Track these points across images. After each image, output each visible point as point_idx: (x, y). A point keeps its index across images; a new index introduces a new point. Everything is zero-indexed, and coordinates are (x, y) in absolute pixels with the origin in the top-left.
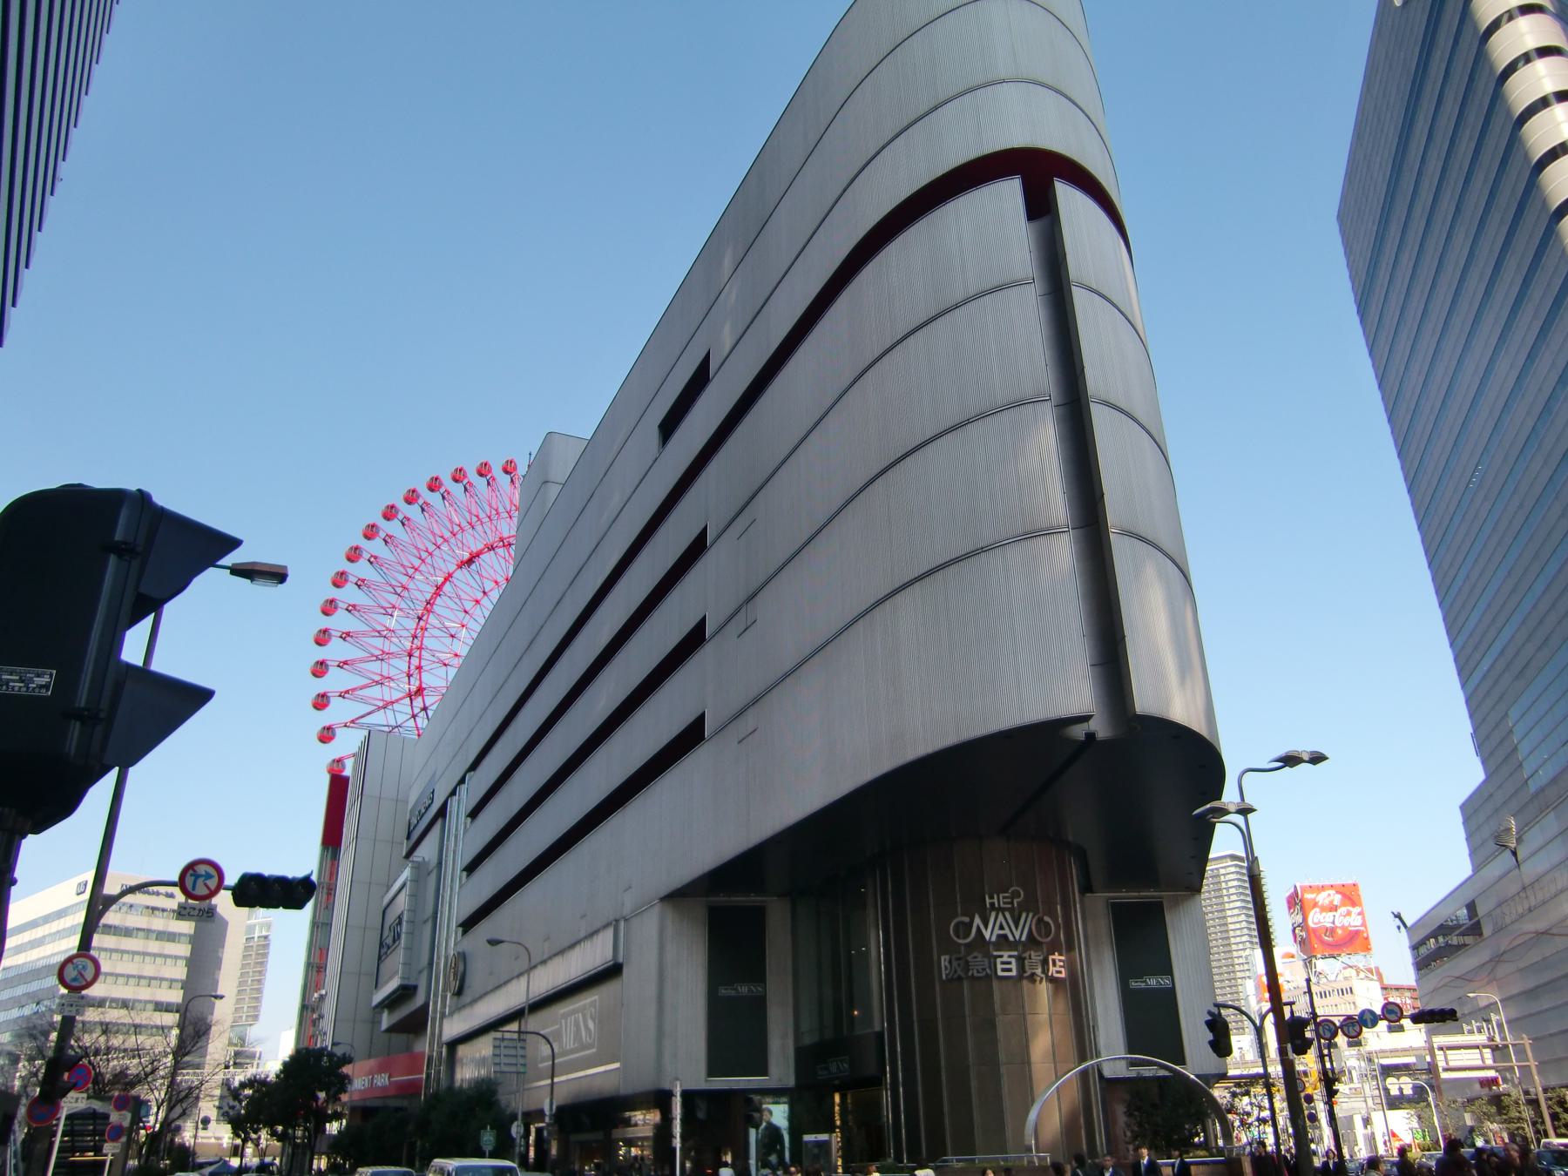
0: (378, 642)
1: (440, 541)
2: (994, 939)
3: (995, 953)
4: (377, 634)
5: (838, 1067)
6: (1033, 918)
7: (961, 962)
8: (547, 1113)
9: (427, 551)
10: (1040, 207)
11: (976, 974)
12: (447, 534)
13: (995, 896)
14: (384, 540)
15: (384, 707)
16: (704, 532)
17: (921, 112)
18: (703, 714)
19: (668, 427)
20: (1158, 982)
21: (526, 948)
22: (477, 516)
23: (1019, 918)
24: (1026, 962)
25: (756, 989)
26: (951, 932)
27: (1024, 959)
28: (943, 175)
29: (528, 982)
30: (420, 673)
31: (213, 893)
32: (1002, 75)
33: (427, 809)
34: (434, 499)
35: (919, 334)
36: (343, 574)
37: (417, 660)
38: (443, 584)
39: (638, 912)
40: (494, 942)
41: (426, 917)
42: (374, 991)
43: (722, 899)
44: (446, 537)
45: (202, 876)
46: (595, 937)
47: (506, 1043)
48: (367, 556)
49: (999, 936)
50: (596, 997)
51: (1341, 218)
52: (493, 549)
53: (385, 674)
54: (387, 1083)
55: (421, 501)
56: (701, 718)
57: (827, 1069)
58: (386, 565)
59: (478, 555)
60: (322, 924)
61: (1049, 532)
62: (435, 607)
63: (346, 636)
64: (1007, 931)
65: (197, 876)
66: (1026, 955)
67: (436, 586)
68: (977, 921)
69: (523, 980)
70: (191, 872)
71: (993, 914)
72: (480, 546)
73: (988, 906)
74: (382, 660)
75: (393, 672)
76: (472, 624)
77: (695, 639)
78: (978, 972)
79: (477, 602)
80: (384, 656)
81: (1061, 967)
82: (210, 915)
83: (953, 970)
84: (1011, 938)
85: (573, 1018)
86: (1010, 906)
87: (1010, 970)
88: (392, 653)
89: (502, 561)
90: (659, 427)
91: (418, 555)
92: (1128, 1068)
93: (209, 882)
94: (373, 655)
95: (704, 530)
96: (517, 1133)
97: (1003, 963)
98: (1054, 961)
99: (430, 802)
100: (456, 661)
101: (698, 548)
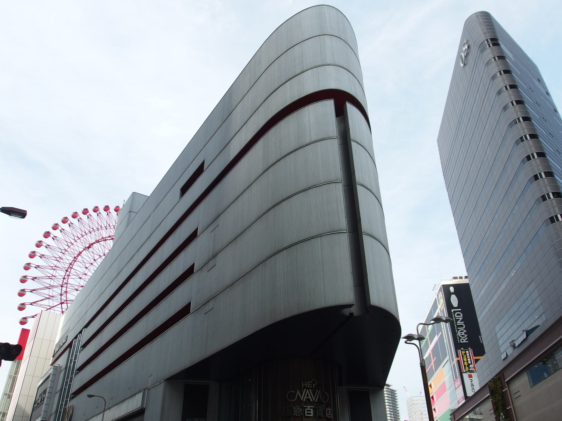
0: (51, 272)
1: (76, 239)
2: (304, 400)
3: (305, 406)
4: (48, 278)
6: (320, 392)
10: (341, 113)
11: (296, 415)
12: (80, 236)
13: (306, 382)
14: (53, 238)
16: (197, 230)
18: (190, 303)
19: (184, 190)
21: (104, 399)
23: (315, 392)
26: (287, 396)
27: (316, 409)
28: (304, 97)
30: (66, 294)
32: (328, 63)
35: (291, 155)
36: (34, 252)
37: (65, 288)
38: (82, 251)
40: (90, 396)
41: (57, 391)
46: (134, 397)
49: (306, 399)
51: (438, 141)
52: (99, 242)
55: (69, 222)
56: (189, 304)
58: (53, 249)
59: (92, 244)
61: (338, 232)
63: (37, 267)
64: (310, 397)
67: (74, 257)
68: (298, 393)
69: (101, 415)
71: (305, 390)
72: (94, 241)
73: (303, 386)
74: (50, 288)
77: (189, 272)
78: (297, 414)
79: (92, 264)
80: (50, 287)
81: (330, 413)
84: (311, 400)
86: (311, 387)
87: (310, 414)
88: (58, 267)
89: (102, 247)
90: (181, 189)
91: (67, 245)
95: (197, 229)
97: (307, 411)
99: (65, 341)
100: (104, 257)
101: (194, 236)
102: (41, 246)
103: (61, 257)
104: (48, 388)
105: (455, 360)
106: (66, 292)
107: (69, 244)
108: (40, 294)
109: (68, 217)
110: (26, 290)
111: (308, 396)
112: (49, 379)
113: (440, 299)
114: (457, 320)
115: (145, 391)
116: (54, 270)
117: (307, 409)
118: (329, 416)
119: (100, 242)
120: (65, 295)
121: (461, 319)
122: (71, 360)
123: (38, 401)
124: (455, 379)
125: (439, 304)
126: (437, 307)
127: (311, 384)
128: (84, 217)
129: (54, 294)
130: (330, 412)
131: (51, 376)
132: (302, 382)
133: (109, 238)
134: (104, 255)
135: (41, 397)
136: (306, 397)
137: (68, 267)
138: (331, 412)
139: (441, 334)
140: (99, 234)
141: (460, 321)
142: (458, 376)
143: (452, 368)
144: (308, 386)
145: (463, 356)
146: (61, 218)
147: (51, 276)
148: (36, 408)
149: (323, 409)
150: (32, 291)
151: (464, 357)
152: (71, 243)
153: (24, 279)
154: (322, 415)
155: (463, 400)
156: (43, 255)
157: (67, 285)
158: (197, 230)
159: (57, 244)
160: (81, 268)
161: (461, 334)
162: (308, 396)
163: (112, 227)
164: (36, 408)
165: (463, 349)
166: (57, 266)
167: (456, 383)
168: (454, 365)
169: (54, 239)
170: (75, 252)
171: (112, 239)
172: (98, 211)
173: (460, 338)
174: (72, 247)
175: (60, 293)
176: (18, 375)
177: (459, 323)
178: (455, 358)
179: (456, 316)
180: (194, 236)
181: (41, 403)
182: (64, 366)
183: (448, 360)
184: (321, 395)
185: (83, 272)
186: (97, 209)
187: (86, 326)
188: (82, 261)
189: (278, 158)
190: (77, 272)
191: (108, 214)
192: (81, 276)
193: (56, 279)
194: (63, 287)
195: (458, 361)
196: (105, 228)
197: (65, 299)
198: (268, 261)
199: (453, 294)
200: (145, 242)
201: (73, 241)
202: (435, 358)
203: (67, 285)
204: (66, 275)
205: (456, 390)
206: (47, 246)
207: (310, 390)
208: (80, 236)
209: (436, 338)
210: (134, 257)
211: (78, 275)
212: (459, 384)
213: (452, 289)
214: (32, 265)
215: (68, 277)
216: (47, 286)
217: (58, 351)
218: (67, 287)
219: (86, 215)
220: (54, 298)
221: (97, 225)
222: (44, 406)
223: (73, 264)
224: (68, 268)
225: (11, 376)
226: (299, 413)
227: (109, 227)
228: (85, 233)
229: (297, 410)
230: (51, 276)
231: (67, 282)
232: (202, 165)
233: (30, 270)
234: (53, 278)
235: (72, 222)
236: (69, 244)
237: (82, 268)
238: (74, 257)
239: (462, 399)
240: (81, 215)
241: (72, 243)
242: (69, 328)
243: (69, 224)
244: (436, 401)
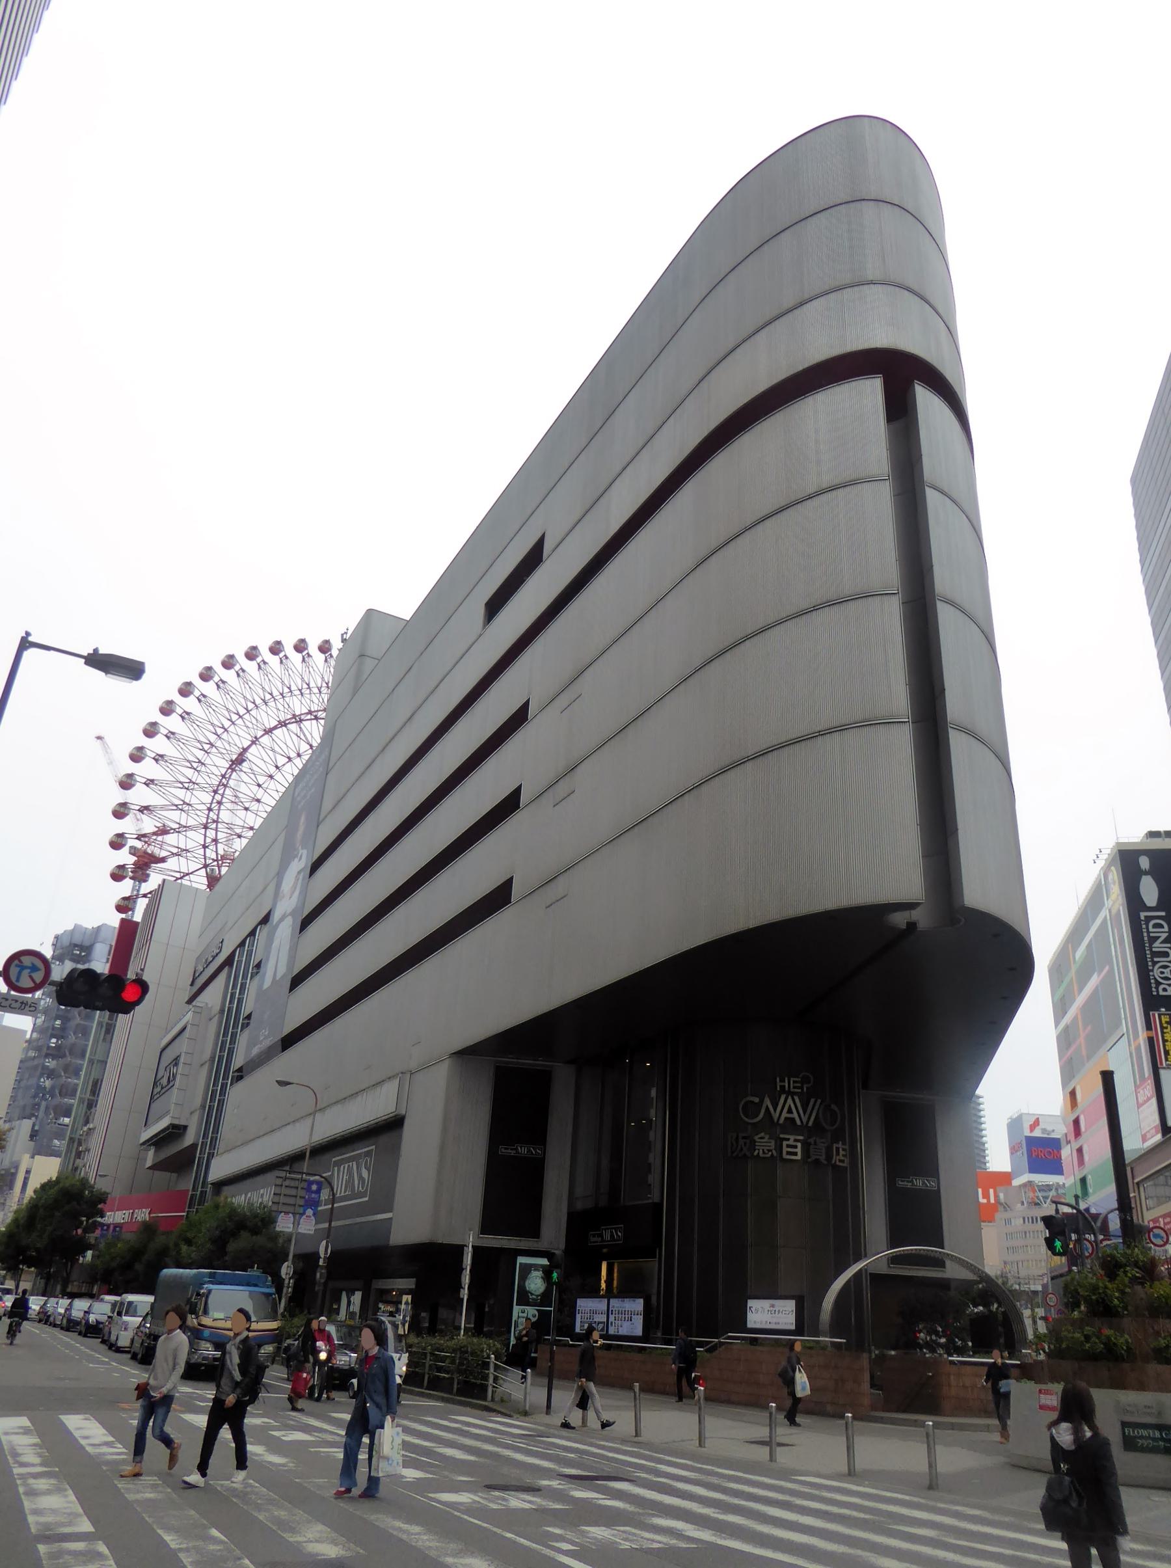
0: (181, 793)
2: (781, 1121)
3: (782, 1136)
4: (175, 808)
5: (612, 1236)
6: (821, 1104)
7: (748, 1141)
8: (322, 1255)
12: (242, 711)
13: (786, 1079)
16: (526, 705)
18: (512, 878)
19: (495, 606)
20: (924, 1183)
23: (807, 1105)
24: (812, 1147)
25: (536, 1151)
29: (313, 1122)
30: (216, 844)
33: (214, 958)
35: (768, 523)
36: (141, 749)
37: (220, 797)
38: (249, 747)
39: (424, 1067)
42: (144, 1129)
43: (510, 1060)
44: (257, 703)
45: (26, 967)
47: (287, 1183)
48: (180, 711)
49: (786, 1119)
51: (1135, 480)
52: (285, 725)
57: (601, 1235)
60: (98, 1061)
61: (889, 722)
63: (149, 783)
64: (795, 1115)
65: (22, 968)
66: (811, 1140)
67: (231, 761)
68: (767, 1102)
70: (16, 962)
71: (783, 1097)
72: (274, 723)
74: (179, 832)
76: (266, 799)
77: (510, 805)
78: (764, 1153)
79: (271, 777)
81: (843, 1155)
82: (33, 1009)
83: (739, 1147)
84: (798, 1122)
85: (347, 1165)
86: (800, 1091)
87: (796, 1154)
88: (197, 784)
89: (295, 737)
92: (889, 1267)
93: (35, 975)
97: (788, 1146)
98: (838, 1149)
99: (218, 951)
101: (519, 718)
103: (202, 761)
104: (183, 1054)
105: (1143, 1035)
106: (215, 841)
107: (220, 731)
109: (213, 667)
111: (790, 1111)
112: (184, 1033)
113: (1112, 886)
114: (1153, 940)
115: (407, 1075)
116: (187, 789)
117: (788, 1142)
118: (840, 1161)
119: (289, 726)
120: (212, 847)
121: (1164, 936)
122: (233, 995)
123: (161, 1081)
124: (1138, 1083)
125: (1107, 899)
126: (1104, 905)
127: (799, 1085)
128: (251, 667)
129: (190, 845)
130: (842, 1152)
131: (189, 1027)
132: (778, 1079)
133: (309, 717)
134: (299, 755)
135: (168, 1071)
136: (785, 1114)
137: (218, 783)
138: (844, 1153)
139: (1108, 972)
140: (286, 706)
141: (1159, 937)
142: (1147, 1075)
143: (1131, 1054)
144: (792, 1090)
145: (1162, 1028)
147: (182, 803)
148: (158, 1095)
149: (826, 1145)
151: (1165, 1031)
152: (223, 728)
153: (122, 810)
154: (823, 1158)
155: (1157, 1133)
156: (162, 756)
157: (217, 825)
158: (526, 705)
159: (192, 729)
160: (323, 820)
161: (1162, 973)
162: (790, 1111)
163: (316, 690)
164: (158, 1095)
165: (1163, 1010)
166: (194, 780)
167: (1141, 1091)
168: (1138, 1048)
169: (183, 718)
170: (233, 750)
171: (316, 718)
172: (281, 651)
173: (1158, 984)
174: (225, 736)
175: (203, 843)
176: (116, 1021)
177: (1158, 946)
178: (1143, 1032)
179: (1151, 929)
180: (519, 718)
181: (168, 1085)
182: (218, 1008)
183: (1123, 1035)
184: (820, 1112)
185: (253, 796)
188: (250, 771)
189: (735, 530)
191: (304, 660)
192: (247, 805)
193: (192, 812)
194: (208, 830)
195: (1151, 1041)
196: (298, 692)
197: (214, 856)
198: (704, 788)
199: (1146, 873)
200: (398, 732)
201: (227, 724)
202: (1089, 1028)
203: (217, 825)
204: (215, 801)
205: (1138, 1108)
206: (170, 735)
207: (796, 1098)
208: (242, 711)
209: (1094, 981)
211: (242, 802)
212: (1149, 1095)
213: (1144, 863)
214: (138, 778)
215: (219, 807)
216: (174, 827)
217: (201, 973)
219: (255, 662)
220: (188, 854)
221: (279, 685)
222: (175, 1091)
223: (230, 776)
224: (219, 785)
225: (102, 1022)
226: (769, 1151)
227: (308, 691)
228: (254, 705)
229: (764, 1144)
230: (182, 803)
231: (218, 818)
232: (540, 545)
233: (134, 789)
234: (186, 808)
235: (224, 680)
236: (220, 731)
239: (1154, 1130)
240: (265, 654)
241: (226, 727)
242: (226, 923)
244: (1086, 1130)
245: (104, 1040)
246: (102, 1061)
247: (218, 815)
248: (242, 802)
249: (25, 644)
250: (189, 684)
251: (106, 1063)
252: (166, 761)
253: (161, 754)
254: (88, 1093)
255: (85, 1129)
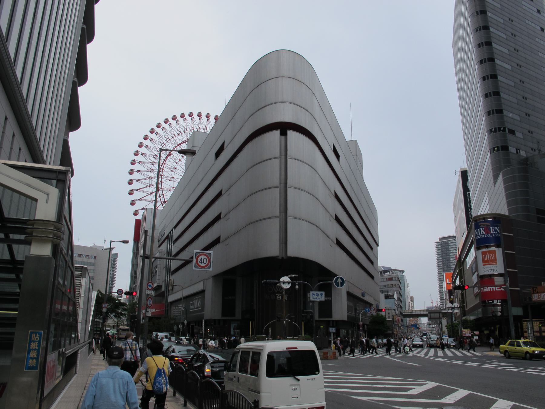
2: (277, 292)
3: (277, 295)
4: (148, 171)
9: (169, 139)
15: (151, 194)
17: (263, 106)
18: (220, 236)
19: (218, 154)
22: (180, 132)
30: (161, 183)
31: (122, 294)
34: (166, 126)
36: (137, 151)
37: (161, 179)
47: (176, 309)
48: (145, 145)
50: (201, 296)
53: (151, 184)
54: (155, 311)
60: (135, 264)
61: (275, 217)
62: (166, 161)
63: (140, 162)
64: (280, 290)
72: (181, 142)
74: (150, 179)
75: (154, 168)
76: (176, 176)
79: (180, 160)
81: (38, 337)
84: (280, 291)
87: (279, 298)
88: (155, 163)
94: (147, 178)
96: (181, 327)
101: (220, 194)
102: (138, 154)
108: (143, 183)
110: (133, 180)
111: (278, 289)
116: (152, 164)
136: (277, 290)
146: (156, 124)
150: (137, 181)
153: (134, 162)
156: (144, 154)
185: (171, 176)
186: (183, 115)
187: (175, 227)
190: (170, 166)
191: (192, 119)
210: (250, 92)
214: (136, 161)
218: (162, 178)
220: (152, 186)
224: (163, 163)
237: (168, 172)
238: (167, 155)
240: (171, 121)
243: (162, 129)
245: (136, 259)
246: (136, 264)
247: (162, 173)
248: (170, 169)
249: (111, 242)
250: (146, 135)
251: (138, 264)
252: (145, 155)
253: (144, 153)
254: (136, 251)
255: (134, 285)
